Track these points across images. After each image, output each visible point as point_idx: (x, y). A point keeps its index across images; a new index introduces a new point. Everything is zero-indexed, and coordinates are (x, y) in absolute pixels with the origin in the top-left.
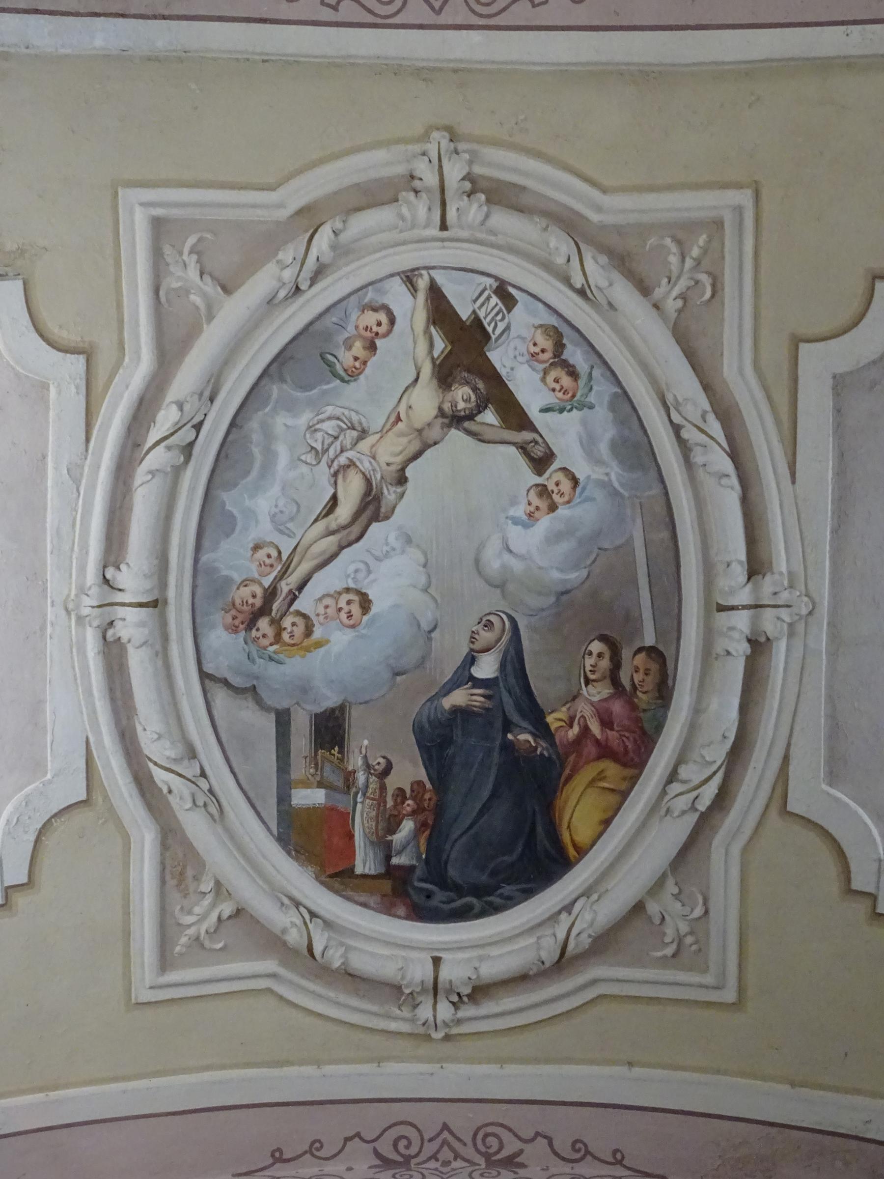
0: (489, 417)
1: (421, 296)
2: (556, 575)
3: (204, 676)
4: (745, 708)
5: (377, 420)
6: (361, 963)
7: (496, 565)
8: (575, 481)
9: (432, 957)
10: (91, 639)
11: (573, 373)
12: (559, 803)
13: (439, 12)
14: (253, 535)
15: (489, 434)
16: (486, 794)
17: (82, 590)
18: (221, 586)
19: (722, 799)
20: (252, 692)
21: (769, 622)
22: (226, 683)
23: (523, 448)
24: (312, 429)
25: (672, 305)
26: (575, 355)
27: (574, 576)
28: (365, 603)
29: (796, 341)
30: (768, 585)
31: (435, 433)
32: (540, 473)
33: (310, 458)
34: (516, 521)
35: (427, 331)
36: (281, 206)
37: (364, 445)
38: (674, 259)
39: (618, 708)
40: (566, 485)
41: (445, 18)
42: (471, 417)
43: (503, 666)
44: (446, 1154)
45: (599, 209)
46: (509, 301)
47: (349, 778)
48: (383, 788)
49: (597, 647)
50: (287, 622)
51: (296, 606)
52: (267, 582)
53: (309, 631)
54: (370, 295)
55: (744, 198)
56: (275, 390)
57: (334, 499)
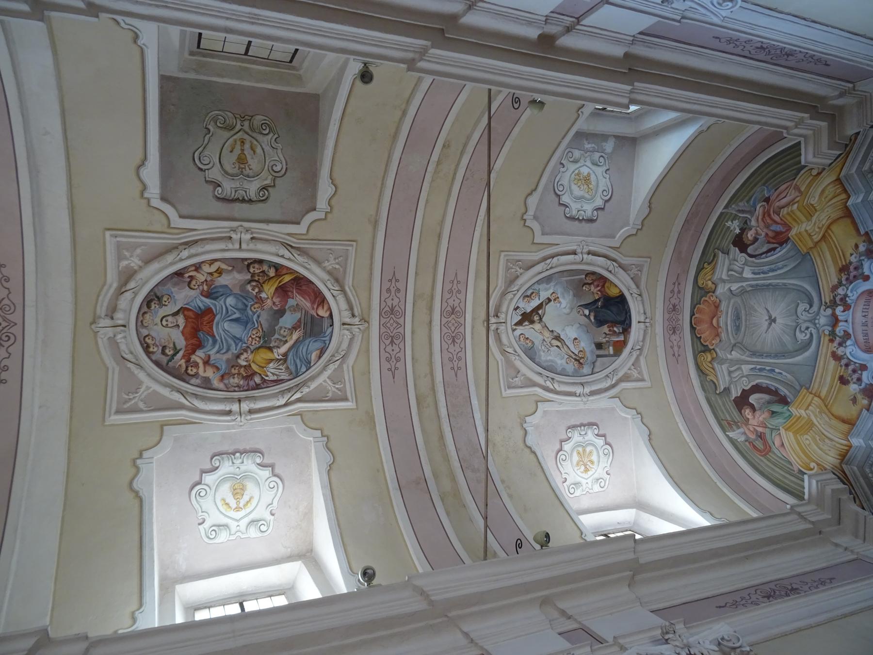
0: (540, 312)
1: (517, 327)
2: (570, 297)
3: (592, 374)
4: (599, 256)
5: (541, 337)
6: (641, 338)
7: (568, 310)
8: (553, 293)
10: (591, 398)
11: (532, 293)
12: (611, 296)
13: (462, 324)
14: (565, 364)
15: (543, 312)
16: (609, 312)
17: (582, 401)
19: (614, 260)
20: (594, 363)
21: (585, 250)
22: (593, 369)
23: (546, 304)
24: (544, 351)
25: (522, 271)
26: (529, 293)
27: (571, 293)
28: (576, 339)
29: (533, 243)
30: (579, 251)
31: (543, 324)
32: (551, 300)
33: (549, 352)
34: (560, 306)
35: (524, 326)
37: (546, 340)
38: (513, 270)
40: (554, 295)
42: (540, 316)
43: (586, 308)
44: (456, 325)
45: (501, 287)
46: (518, 307)
47: (607, 342)
48: (609, 334)
49: (584, 288)
50: (580, 356)
51: (577, 354)
52: (573, 361)
53: (581, 351)
54: (517, 339)
55: (503, 254)
56: (537, 360)
57: (557, 346)
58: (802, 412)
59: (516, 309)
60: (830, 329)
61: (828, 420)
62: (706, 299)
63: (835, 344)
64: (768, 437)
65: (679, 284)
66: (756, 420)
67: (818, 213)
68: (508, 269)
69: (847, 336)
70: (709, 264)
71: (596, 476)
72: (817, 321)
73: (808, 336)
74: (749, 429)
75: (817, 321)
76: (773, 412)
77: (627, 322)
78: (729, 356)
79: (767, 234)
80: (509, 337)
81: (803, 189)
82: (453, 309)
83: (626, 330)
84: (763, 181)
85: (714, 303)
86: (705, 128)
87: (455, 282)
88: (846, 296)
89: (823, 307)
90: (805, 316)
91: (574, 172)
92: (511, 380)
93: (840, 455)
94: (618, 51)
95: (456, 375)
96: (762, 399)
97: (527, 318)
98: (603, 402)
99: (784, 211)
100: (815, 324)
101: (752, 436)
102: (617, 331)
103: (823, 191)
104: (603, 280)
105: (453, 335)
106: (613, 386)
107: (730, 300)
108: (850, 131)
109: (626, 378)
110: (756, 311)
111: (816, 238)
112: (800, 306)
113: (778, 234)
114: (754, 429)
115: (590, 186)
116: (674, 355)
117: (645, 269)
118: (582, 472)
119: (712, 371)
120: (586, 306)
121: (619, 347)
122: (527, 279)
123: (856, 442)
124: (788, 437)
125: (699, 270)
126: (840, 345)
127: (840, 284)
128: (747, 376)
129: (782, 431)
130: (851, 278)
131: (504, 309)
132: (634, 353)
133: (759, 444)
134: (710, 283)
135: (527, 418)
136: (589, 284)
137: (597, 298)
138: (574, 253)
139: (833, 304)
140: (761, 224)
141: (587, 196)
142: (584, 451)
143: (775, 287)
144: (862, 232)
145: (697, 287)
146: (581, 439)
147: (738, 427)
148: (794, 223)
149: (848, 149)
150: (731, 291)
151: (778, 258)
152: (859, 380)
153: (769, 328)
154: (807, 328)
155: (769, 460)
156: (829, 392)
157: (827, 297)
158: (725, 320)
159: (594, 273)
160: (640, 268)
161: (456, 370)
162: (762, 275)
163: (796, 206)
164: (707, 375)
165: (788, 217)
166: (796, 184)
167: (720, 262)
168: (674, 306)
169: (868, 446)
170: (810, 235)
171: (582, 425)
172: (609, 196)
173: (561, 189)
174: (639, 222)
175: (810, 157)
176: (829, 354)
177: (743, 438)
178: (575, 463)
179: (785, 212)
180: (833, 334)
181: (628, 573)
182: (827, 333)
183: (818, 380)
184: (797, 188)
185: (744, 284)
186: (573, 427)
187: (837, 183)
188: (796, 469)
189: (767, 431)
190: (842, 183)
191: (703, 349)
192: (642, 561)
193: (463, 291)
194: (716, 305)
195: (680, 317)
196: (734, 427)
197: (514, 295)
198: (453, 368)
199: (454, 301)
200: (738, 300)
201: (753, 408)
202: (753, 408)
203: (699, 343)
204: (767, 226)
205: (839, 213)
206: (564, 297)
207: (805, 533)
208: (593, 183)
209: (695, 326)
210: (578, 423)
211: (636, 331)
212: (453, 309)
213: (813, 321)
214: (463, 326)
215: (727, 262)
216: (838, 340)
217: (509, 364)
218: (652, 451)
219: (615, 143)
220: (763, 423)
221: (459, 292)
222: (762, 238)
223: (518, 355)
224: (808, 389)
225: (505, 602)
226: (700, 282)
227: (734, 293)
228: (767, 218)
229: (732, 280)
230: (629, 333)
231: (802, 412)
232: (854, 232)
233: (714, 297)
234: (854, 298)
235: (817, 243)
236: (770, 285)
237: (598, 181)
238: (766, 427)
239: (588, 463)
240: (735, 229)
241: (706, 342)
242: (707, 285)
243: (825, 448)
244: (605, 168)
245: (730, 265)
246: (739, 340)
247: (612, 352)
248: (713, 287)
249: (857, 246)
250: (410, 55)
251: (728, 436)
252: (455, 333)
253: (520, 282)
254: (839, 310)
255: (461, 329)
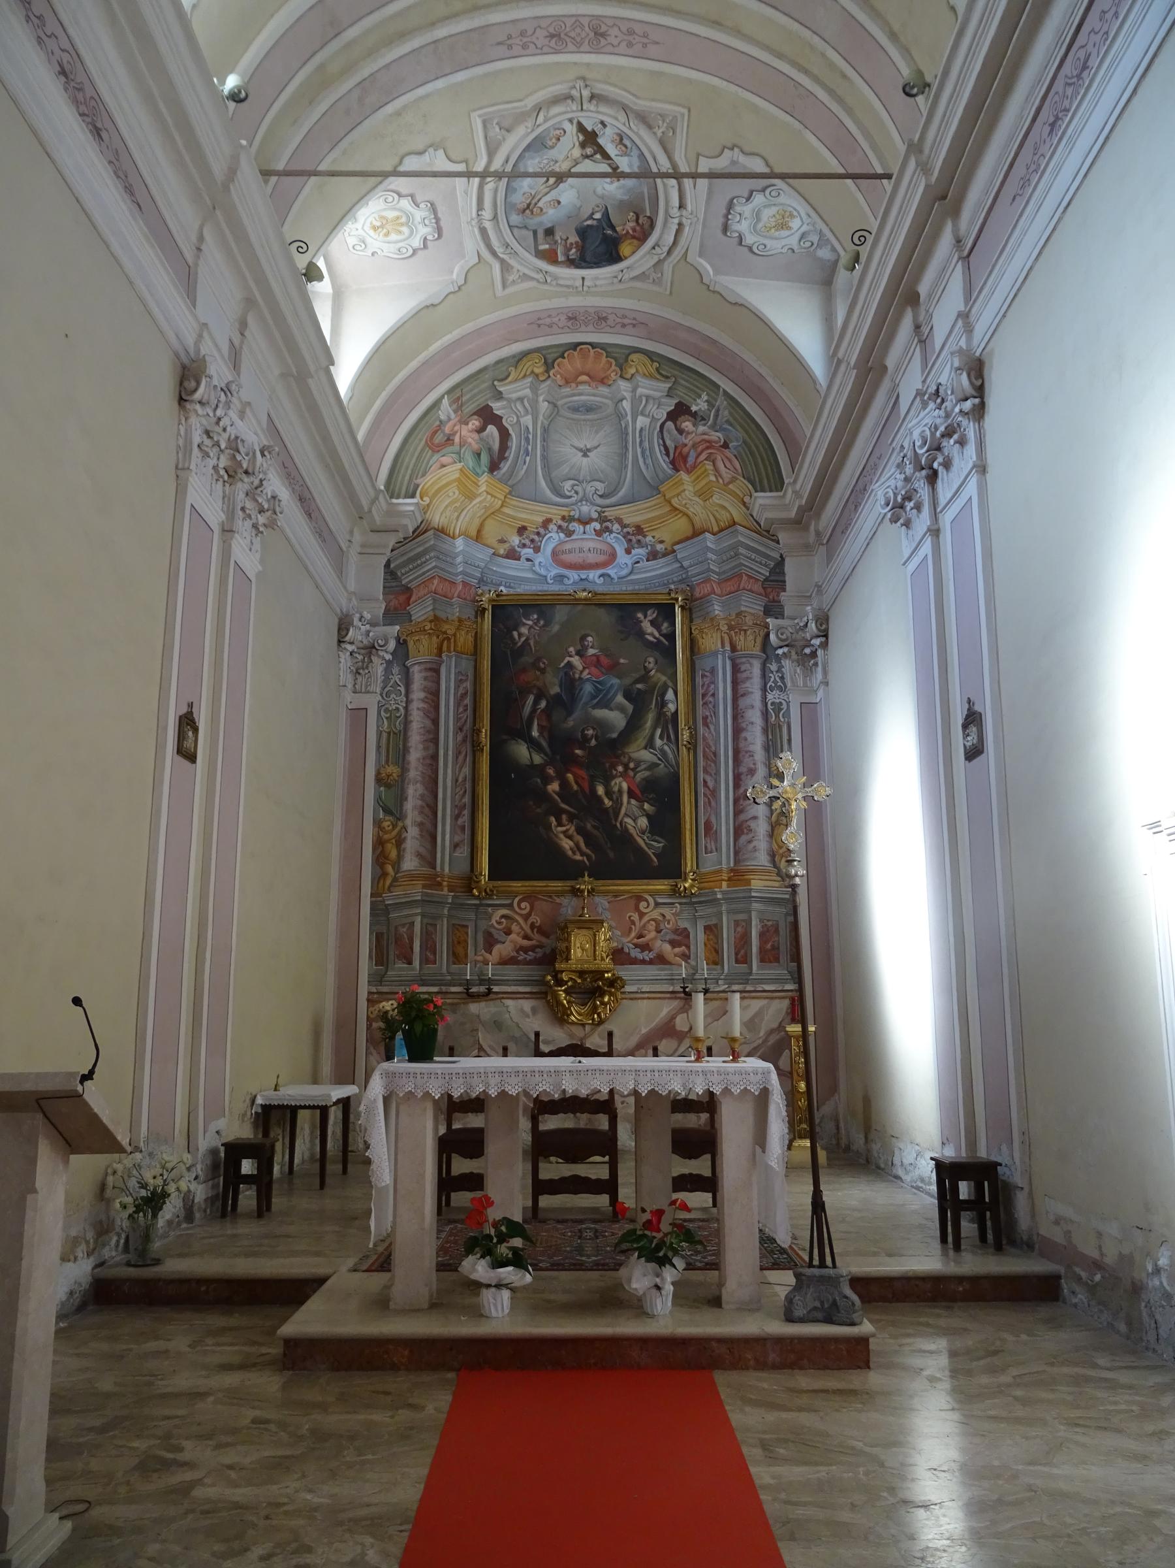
0: (598, 156)
5: (561, 157)
9: (490, 953)
10: (476, 231)
11: (626, 146)
17: (472, 219)
18: (513, 206)
19: (669, 252)
20: (526, 227)
21: (684, 220)
24: (539, 162)
25: (659, 134)
27: (626, 198)
28: (559, 202)
29: (698, 155)
30: (684, 213)
31: (581, 159)
36: (526, 106)
37: (558, 165)
39: (638, 228)
41: (582, 49)
42: (592, 156)
43: (603, 215)
44: (578, 39)
47: (556, 242)
49: (632, 214)
53: (542, 210)
54: (557, 126)
55: (686, 111)
56: (527, 154)
58: (483, 488)
59: (602, 123)
60: (576, 517)
61: (479, 515)
62: (613, 367)
63: (560, 522)
64: (450, 449)
65: (634, 326)
66: (467, 432)
67: (701, 502)
68: (663, 116)
69: (569, 533)
70: (657, 369)
71: (369, 240)
72: (584, 503)
73: (568, 494)
74: (455, 426)
75: (584, 503)
76: (479, 455)
77: (583, 264)
78: (541, 398)
79: (686, 445)
80: (561, 115)
81: (731, 486)
82: (603, 35)
83: (571, 263)
84: (748, 440)
85: (607, 377)
86: (818, 387)
87: (645, 40)
88: (611, 532)
89: (599, 509)
90: (590, 489)
91: (795, 210)
92: (495, 121)
93: (443, 528)
94: (891, 362)
95: (499, 44)
96: (494, 441)
97: (589, 139)
98: (472, 244)
99: (709, 466)
100: (581, 501)
101: (447, 429)
102: (571, 253)
103: (724, 508)
104: (642, 235)
105: (562, 36)
106: (494, 253)
107: (611, 399)
108: (781, 536)
109: (505, 267)
110: (597, 432)
111: (675, 502)
112: (602, 485)
113: (685, 458)
114: (457, 432)
115: (773, 230)
116: (538, 323)
117: (655, 288)
118: (371, 223)
119: (522, 375)
120: (606, 214)
121: (550, 257)
122: (648, 141)
123: (460, 543)
124: (453, 471)
125: (650, 355)
126: (560, 527)
127: (624, 526)
128: (518, 421)
129: (459, 466)
130: (629, 537)
131: (602, 109)
132: (541, 275)
133: (439, 438)
134: (633, 371)
135: (441, 151)
136: (637, 221)
137: (618, 229)
138: (682, 206)
139: (602, 519)
140: (698, 439)
141: (760, 225)
142: (402, 224)
143: (623, 455)
144: (676, 547)
145: (627, 352)
146: (418, 219)
147: (455, 411)
148: (693, 478)
149: (765, 533)
150: (622, 400)
151: (657, 458)
152: (524, 546)
153: (576, 448)
154: (577, 493)
155: (422, 450)
156: (509, 516)
157: (610, 513)
158: (586, 393)
159: (652, 226)
160: (658, 282)
161: (506, 43)
162: (638, 440)
163: (713, 479)
164: (516, 368)
165: (703, 469)
166: (737, 479)
167: (659, 384)
168: (605, 319)
169: (457, 555)
170: (678, 495)
171: (437, 220)
172: (756, 251)
173: (773, 193)
174: (717, 289)
175: (760, 501)
176: (549, 516)
177: (443, 417)
178: (384, 214)
179: (707, 467)
180: (571, 519)
181: (294, 370)
182: (572, 513)
183: (521, 505)
184: (733, 480)
185: (629, 418)
186: (434, 209)
187: (731, 522)
188: (418, 481)
189: (456, 448)
190: (730, 527)
191: (550, 361)
192: (310, 381)
193: (630, 51)
194: (606, 381)
195: (591, 328)
196: (455, 406)
197: (624, 124)
198: (510, 37)
199: (616, 37)
200: (610, 410)
201: (481, 430)
202: (481, 430)
203: (556, 355)
204: (694, 446)
205: (698, 525)
206: (617, 188)
207: (358, 506)
208: (777, 233)
209: (578, 349)
210: (440, 215)
211: (574, 274)
212: (603, 35)
213: (584, 499)
214: (576, 50)
215: (657, 394)
216: (565, 525)
217: (521, 117)
218: (414, 312)
219: (829, 261)
220: (465, 442)
221: (630, 45)
222: (683, 439)
223: (533, 130)
224: (510, 493)
225: (242, 264)
226: (634, 357)
227: (620, 404)
228: (705, 446)
229: (635, 401)
230: (569, 267)
231: (483, 488)
232: (677, 539)
233: (614, 378)
234: (609, 540)
235: (670, 502)
236: (627, 449)
237: (776, 239)
238: (461, 446)
239: (385, 230)
240: (697, 405)
241: (558, 365)
242: (631, 366)
243: (448, 513)
244: (796, 248)
245: (654, 399)
246: (562, 412)
247: (542, 247)
248: (629, 376)
249: (662, 542)
250: (927, 151)
251: (443, 397)
252: (566, 38)
253: (643, 132)
254: (597, 526)
255: (571, 47)
